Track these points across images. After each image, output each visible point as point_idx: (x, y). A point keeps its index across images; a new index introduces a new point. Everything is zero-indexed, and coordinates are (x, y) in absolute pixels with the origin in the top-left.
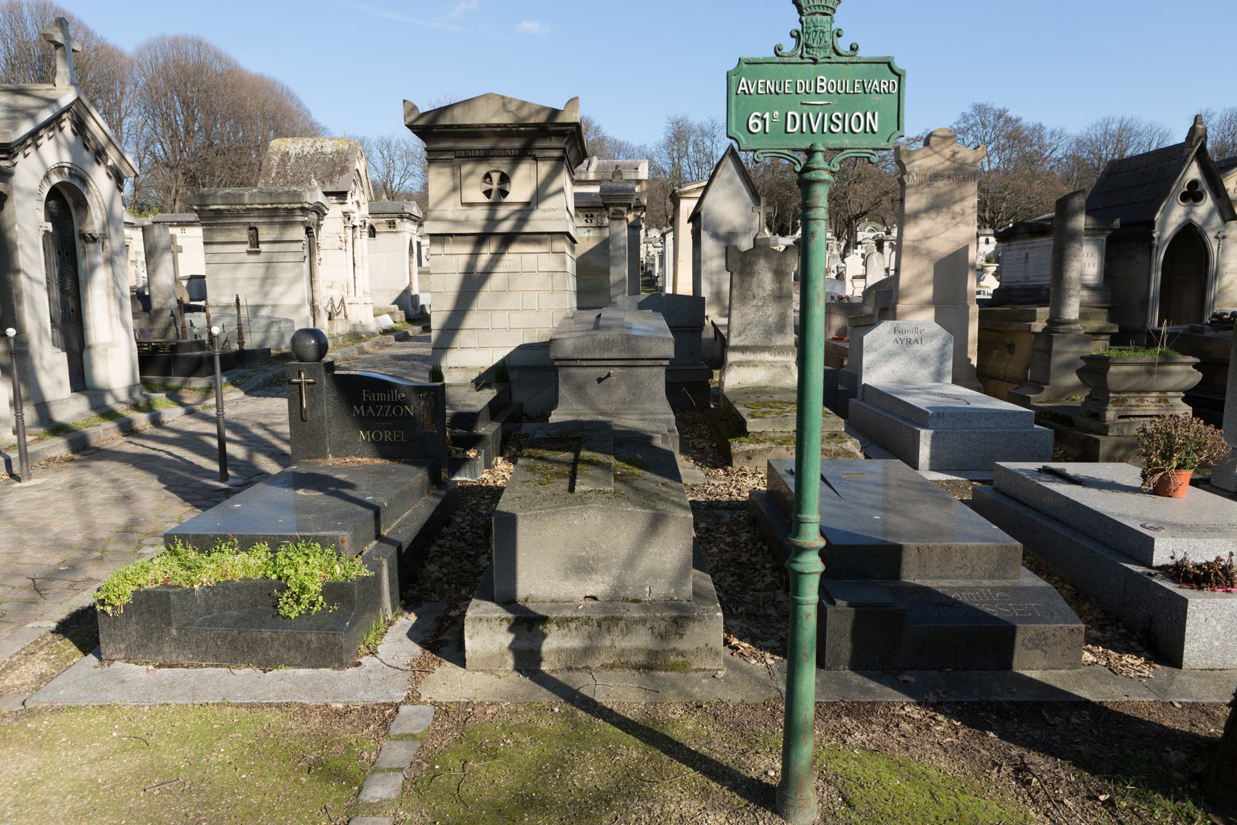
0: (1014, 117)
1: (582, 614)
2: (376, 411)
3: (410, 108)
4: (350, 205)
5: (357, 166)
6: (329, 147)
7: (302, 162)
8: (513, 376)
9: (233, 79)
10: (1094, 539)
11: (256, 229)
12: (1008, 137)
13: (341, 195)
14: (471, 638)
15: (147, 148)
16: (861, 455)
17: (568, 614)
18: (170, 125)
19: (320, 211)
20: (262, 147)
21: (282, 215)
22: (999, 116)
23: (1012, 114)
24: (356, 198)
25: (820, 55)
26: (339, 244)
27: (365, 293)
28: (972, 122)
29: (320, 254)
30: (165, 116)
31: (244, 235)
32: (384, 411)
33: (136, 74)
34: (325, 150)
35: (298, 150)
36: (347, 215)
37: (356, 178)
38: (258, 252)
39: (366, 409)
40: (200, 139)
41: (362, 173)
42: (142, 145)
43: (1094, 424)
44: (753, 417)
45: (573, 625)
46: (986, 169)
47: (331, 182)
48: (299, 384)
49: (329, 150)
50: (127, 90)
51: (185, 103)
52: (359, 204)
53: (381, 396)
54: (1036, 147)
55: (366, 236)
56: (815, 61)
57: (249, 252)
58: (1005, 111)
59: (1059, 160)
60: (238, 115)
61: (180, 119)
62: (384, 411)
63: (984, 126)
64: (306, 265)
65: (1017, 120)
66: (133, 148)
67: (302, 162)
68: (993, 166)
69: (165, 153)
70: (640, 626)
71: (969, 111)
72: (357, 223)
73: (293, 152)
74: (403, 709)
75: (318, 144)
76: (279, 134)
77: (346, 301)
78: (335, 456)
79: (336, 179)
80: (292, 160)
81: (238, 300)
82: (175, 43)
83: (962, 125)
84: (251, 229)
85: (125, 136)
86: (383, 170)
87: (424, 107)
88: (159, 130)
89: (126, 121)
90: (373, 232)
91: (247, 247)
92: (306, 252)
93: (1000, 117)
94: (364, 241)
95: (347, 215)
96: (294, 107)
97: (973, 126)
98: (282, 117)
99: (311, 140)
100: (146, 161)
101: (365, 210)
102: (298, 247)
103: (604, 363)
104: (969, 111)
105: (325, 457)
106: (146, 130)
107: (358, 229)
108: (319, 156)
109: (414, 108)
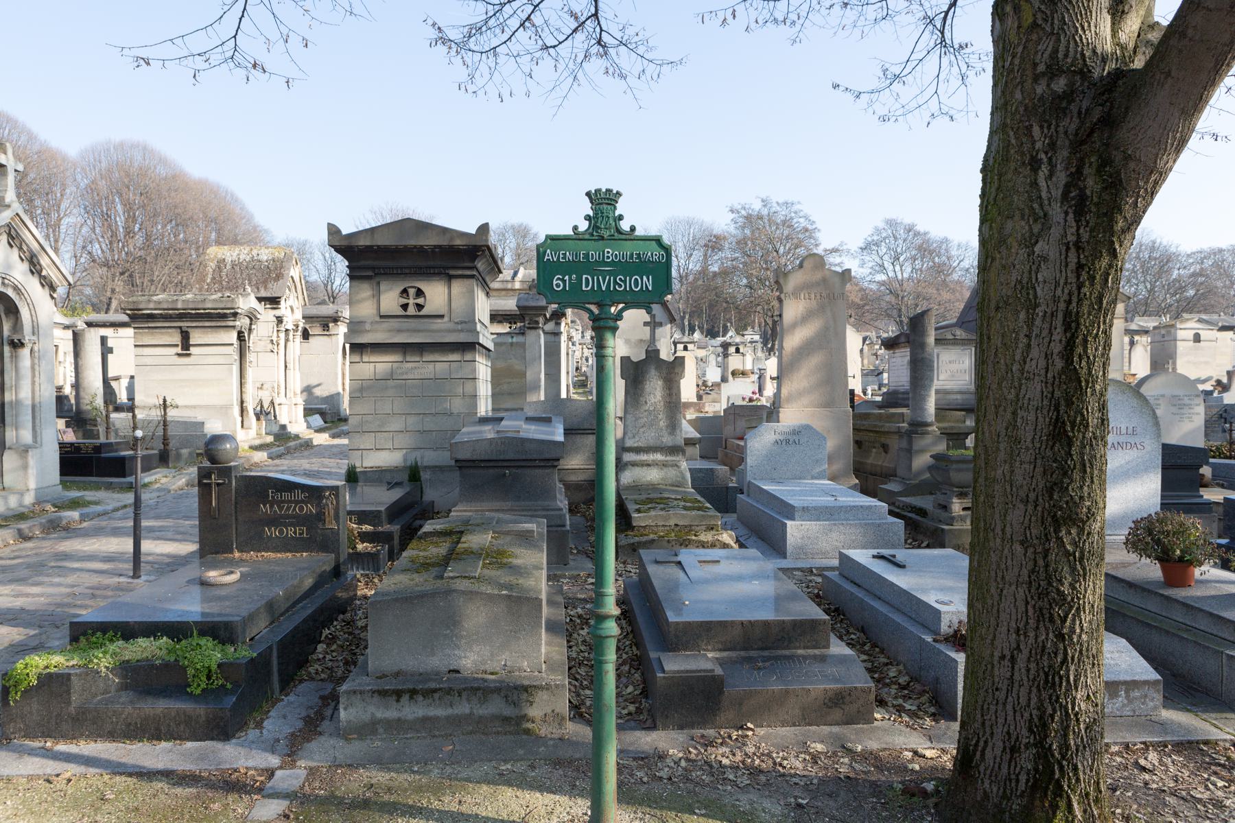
0: (922, 231)
1: (445, 685)
2: (281, 508)
3: (333, 231)
4: (284, 309)
5: (292, 273)
6: (265, 255)
7: (237, 269)
8: (425, 476)
9: (177, 182)
10: (905, 614)
11: (187, 332)
12: (920, 248)
13: (274, 301)
14: (345, 709)
15: (84, 247)
16: (736, 546)
17: (433, 685)
18: (110, 226)
19: (252, 317)
20: (201, 249)
21: (220, 318)
22: (909, 229)
23: (920, 228)
24: (289, 303)
25: (606, 234)
26: (270, 346)
27: (295, 394)
28: (884, 235)
29: (250, 357)
30: (106, 217)
31: (177, 339)
32: (288, 508)
33: (79, 177)
34: (260, 257)
35: (235, 258)
36: (280, 320)
37: (290, 283)
38: (189, 355)
39: (271, 507)
40: (139, 239)
41: (297, 279)
42: (80, 242)
43: (944, 515)
44: (638, 511)
45: (436, 695)
46: (900, 277)
47: (266, 288)
48: (210, 485)
49: (265, 258)
50: (68, 191)
51: (129, 207)
52: (293, 310)
53: (286, 496)
54: (944, 258)
55: (299, 338)
56: (602, 238)
57: (179, 355)
58: (914, 226)
59: (967, 270)
60: (180, 221)
61: (121, 221)
62: (288, 508)
63: (896, 239)
64: (235, 368)
65: (925, 234)
66: (70, 247)
67: (237, 269)
68: (906, 275)
69: (103, 251)
70: (496, 695)
71: (881, 225)
72: (290, 326)
73: (228, 260)
74: (279, 773)
75: (255, 252)
76: (219, 243)
77: (276, 402)
78: (241, 551)
79: (270, 285)
80: (228, 267)
81: (165, 401)
82: (121, 146)
83: (875, 238)
84: (182, 332)
85: (62, 236)
86: (324, 272)
87: (345, 231)
88: (98, 230)
89: (65, 221)
90: (306, 335)
91: (179, 350)
92: (237, 357)
93: (909, 231)
94: (296, 342)
95: (280, 320)
96: (238, 211)
97: (885, 238)
98: (224, 222)
99: (248, 249)
100: (83, 260)
101: (298, 315)
102: (229, 350)
103: (500, 464)
104: (881, 225)
105: (231, 552)
106: (85, 230)
107: (291, 333)
108: (254, 265)
109: (339, 231)
